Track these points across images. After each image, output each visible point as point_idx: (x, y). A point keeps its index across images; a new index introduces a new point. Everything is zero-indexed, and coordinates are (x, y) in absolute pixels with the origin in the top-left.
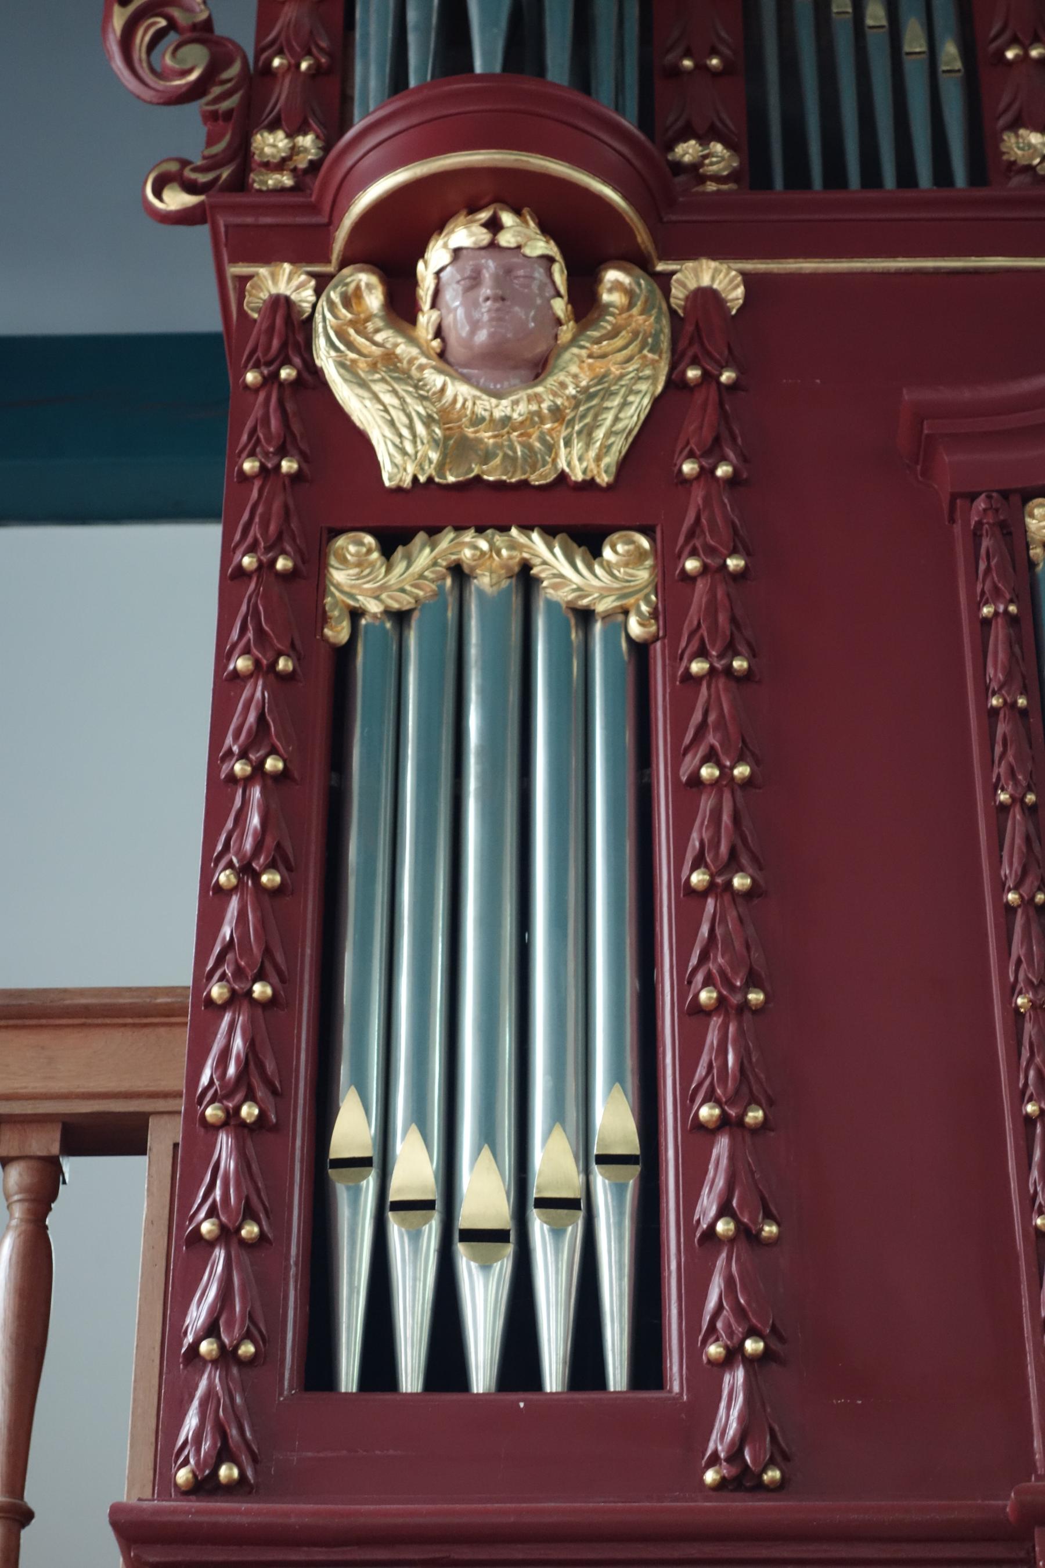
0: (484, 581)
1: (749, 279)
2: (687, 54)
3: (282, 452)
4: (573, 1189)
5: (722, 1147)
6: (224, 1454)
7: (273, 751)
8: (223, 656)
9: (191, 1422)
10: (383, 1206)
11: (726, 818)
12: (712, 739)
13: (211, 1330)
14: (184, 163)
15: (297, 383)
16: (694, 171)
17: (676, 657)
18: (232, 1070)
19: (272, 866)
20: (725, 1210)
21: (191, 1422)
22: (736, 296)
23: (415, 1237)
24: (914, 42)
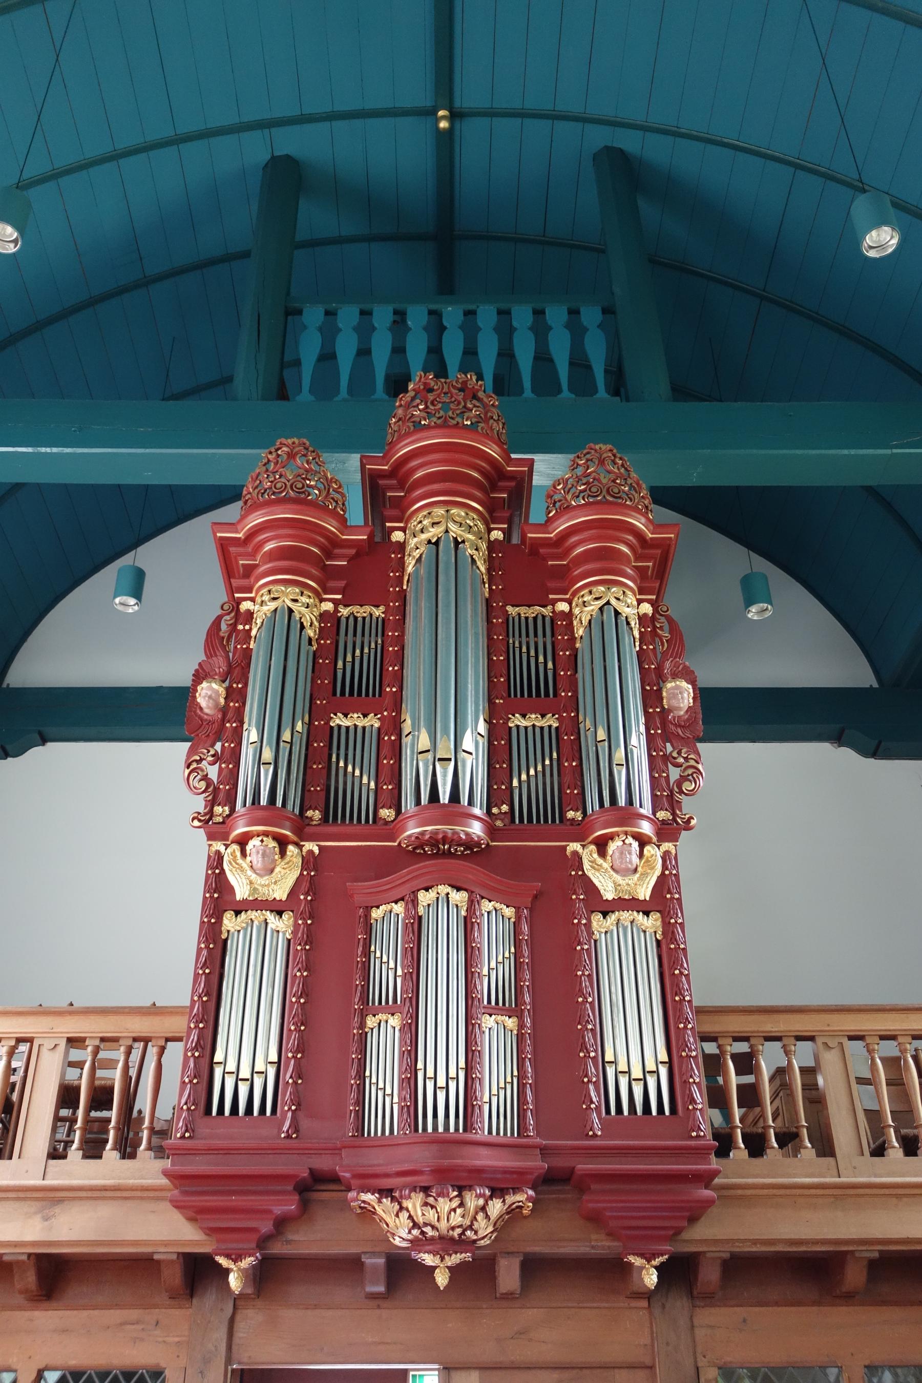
0: (256, 923)
1: (320, 847)
2: (312, 786)
3: (215, 892)
4: (263, 1070)
5: (292, 1062)
6: (187, 1131)
7: (207, 968)
8: (199, 943)
9: (181, 1124)
10: (224, 1073)
11: (301, 985)
12: (300, 965)
13: (186, 1103)
14: (199, 813)
15: (219, 873)
16: (311, 819)
17: (295, 944)
18: (194, 1045)
19: (205, 995)
20: (291, 1077)
21: (181, 1124)
22: (316, 850)
23: (445, 770)
24: (365, 780)
